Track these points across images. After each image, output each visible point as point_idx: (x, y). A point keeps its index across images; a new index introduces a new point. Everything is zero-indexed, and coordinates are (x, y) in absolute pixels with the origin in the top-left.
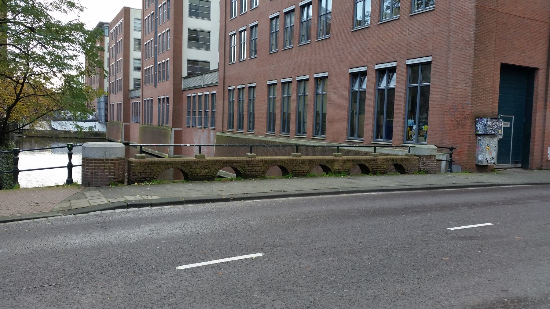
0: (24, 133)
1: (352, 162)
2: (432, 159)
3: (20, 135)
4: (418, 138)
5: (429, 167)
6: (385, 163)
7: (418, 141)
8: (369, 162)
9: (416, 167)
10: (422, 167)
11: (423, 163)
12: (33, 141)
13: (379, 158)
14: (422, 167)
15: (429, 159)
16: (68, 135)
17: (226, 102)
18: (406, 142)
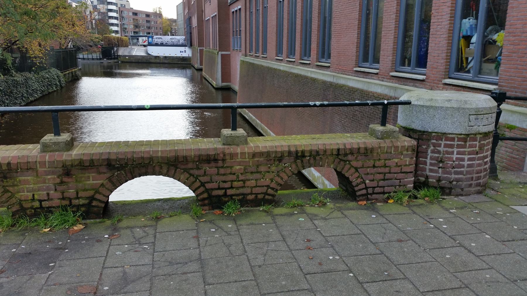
0: (119, 59)
1: (103, 169)
2: (471, 146)
3: (116, 61)
4: (481, 66)
5: (456, 173)
6: (263, 169)
7: (480, 73)
8: (190, 165)
9: (401, 176)
10: (431, 171)
11: (436, 159)
12: (128, 66)
13: (239, 150)
14: (431, 171)
15: (458, 146)
16: (158, 61)
17: (248, 13)
18: (453, 76)
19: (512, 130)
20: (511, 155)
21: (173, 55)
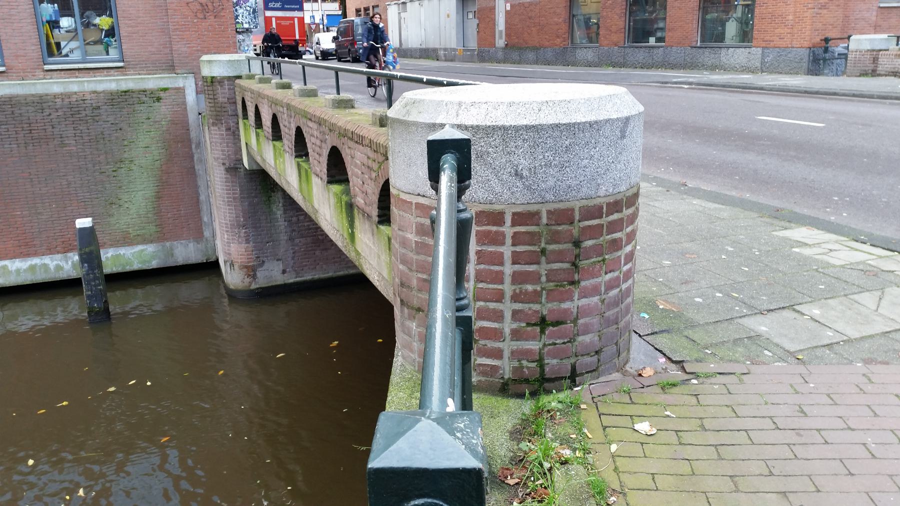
19: (166, 92)
20: (173, 110)
21: (246, 158)
